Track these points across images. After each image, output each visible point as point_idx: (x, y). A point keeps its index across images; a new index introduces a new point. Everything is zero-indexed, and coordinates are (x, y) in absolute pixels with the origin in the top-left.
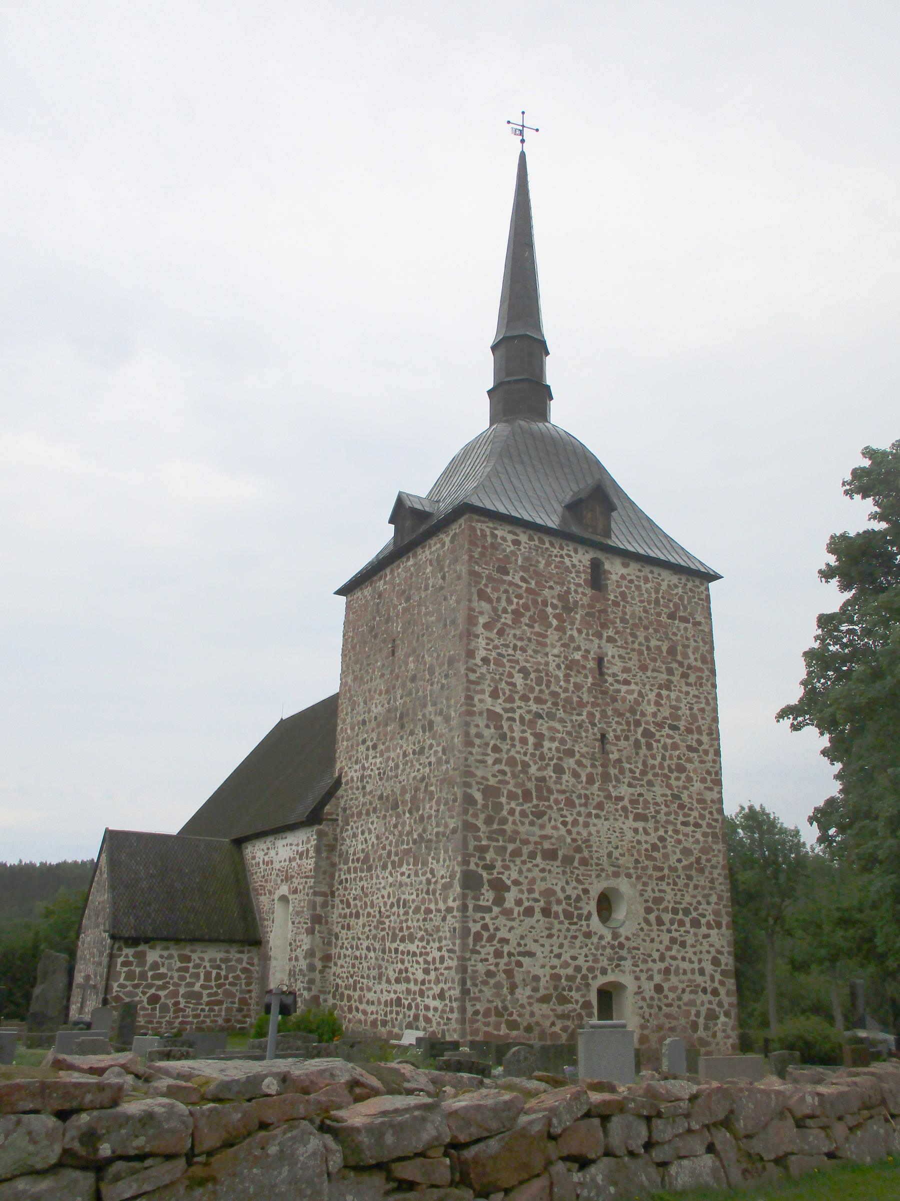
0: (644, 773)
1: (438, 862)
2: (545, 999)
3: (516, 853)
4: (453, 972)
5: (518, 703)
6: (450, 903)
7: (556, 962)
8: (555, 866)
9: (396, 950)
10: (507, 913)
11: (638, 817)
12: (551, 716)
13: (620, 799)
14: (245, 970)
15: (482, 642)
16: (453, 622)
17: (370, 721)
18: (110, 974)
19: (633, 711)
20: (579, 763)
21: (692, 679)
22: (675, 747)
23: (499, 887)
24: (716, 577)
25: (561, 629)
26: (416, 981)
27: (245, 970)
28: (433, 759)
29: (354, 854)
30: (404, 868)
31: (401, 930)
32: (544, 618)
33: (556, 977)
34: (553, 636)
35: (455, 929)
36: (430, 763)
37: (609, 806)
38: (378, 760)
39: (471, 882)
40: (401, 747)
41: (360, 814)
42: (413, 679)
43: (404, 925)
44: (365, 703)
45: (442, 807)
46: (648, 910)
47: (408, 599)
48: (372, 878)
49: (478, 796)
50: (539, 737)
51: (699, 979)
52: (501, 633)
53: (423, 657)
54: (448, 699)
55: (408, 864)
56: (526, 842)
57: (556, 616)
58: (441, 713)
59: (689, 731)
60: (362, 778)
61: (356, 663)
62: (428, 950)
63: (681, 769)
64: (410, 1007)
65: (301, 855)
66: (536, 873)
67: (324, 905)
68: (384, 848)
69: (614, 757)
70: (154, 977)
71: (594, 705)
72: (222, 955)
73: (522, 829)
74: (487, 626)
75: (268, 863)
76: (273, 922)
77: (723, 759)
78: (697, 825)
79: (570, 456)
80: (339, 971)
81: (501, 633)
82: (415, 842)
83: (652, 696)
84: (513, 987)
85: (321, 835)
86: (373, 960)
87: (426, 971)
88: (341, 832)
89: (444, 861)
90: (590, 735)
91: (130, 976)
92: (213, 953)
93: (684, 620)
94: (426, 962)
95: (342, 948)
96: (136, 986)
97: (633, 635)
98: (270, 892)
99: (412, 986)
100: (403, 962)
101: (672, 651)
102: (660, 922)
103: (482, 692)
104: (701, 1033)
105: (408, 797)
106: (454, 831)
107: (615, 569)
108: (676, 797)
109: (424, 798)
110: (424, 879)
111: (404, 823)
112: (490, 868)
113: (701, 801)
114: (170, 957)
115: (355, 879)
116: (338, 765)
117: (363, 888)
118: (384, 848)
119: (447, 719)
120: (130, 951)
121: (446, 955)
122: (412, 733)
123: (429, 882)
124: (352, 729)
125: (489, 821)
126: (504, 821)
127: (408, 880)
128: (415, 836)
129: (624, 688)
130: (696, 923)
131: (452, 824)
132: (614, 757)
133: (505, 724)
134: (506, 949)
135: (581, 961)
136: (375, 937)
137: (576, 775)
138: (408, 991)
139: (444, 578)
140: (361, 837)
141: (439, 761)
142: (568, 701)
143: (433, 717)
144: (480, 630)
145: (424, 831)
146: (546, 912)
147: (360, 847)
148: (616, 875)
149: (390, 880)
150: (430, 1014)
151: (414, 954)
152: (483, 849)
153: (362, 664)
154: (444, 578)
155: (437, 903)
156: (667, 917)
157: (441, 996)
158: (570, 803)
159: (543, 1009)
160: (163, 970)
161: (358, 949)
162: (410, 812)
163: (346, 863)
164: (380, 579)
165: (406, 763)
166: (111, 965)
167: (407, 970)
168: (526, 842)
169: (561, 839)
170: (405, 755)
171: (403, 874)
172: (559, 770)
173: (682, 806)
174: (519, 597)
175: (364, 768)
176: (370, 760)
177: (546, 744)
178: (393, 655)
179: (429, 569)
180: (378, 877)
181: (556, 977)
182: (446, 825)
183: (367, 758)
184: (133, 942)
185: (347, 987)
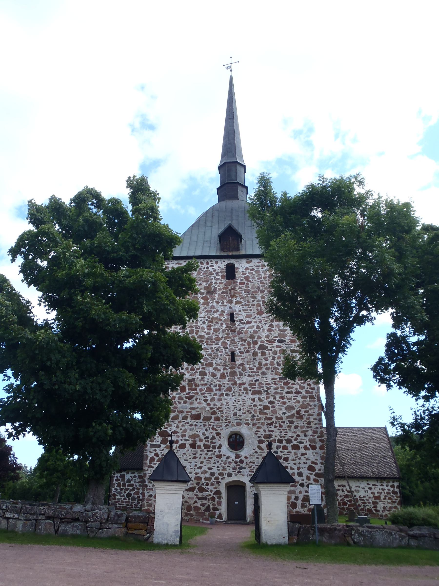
70: (128, 486)
91: (119, 485)
96: (121, 490)
114: (135, 477)
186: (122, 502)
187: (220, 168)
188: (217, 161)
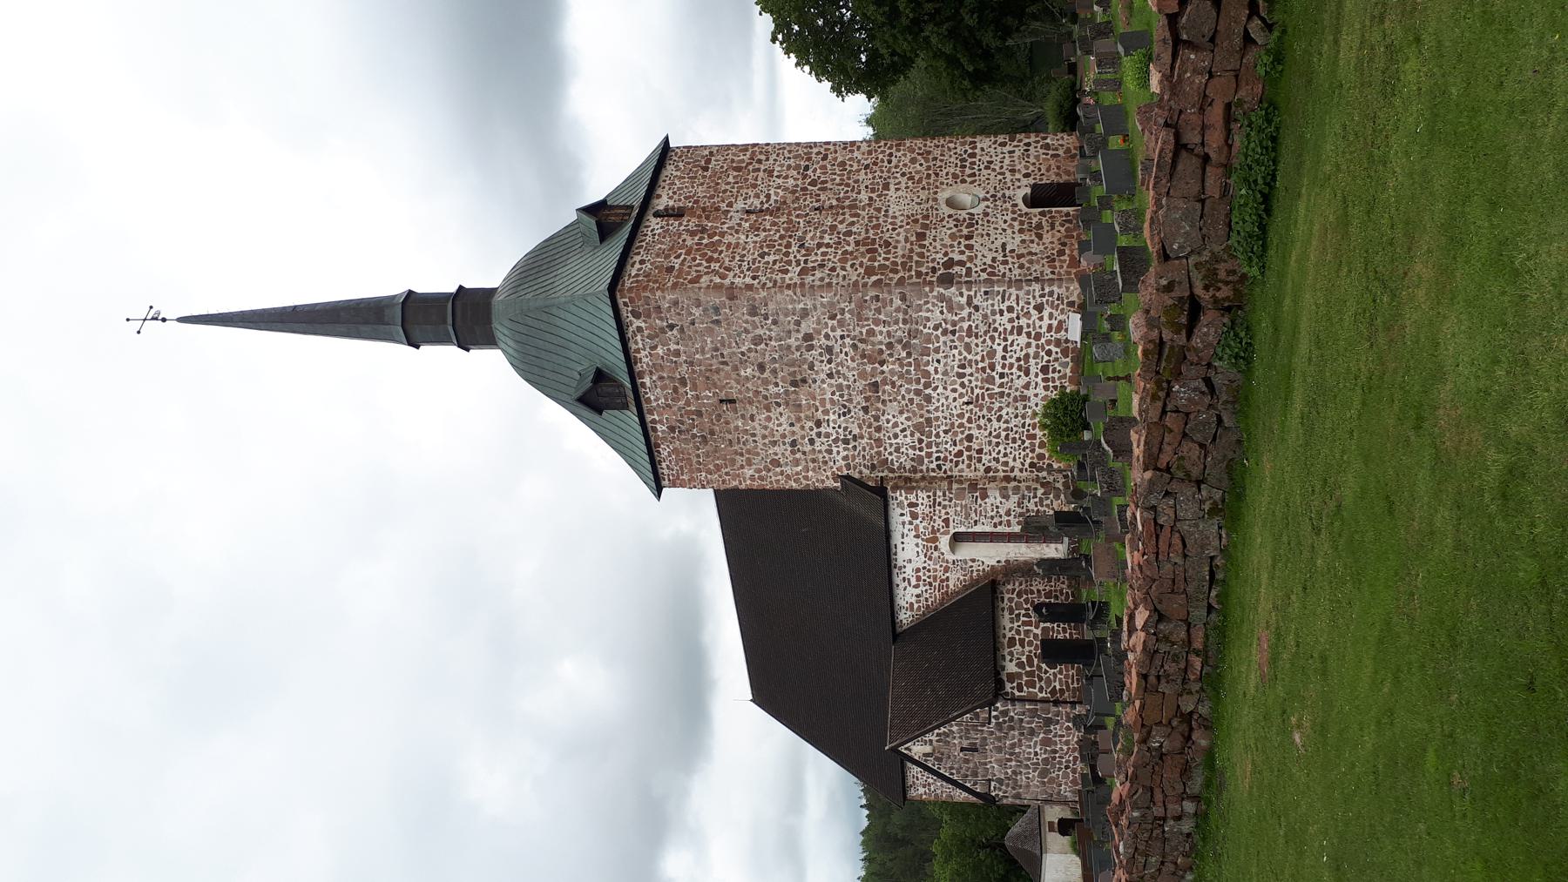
0: (848, 185)
1: (928, 319)
2: (1040, 237)
3: (921, 255)
4: (1021, 293)
5: (791, 257)
6: (964, 300)
7: (1009, 231)
8: (930, 234)
9: (1002, 376)
10: (971, 259)
11: (886, 187)
12: (801, 239)
13: (871, 199)
14: (1019, 595)
15: (737, 280)
16: (717, 310)
17: (793, 433)
18: (1033, 701)
19: (794, 192)
20: (841, 222)
21: (763, 157)
22: (824, 167)
23: (950, 263)
24: (667, 138)
25: (722, 234)
26: (1028, 345)
27: (1019, 595)
28: (839, 333)
29: (914, 448)
30: (931, 369)
31: (983, 369)
32: (713, 246)
33: (1021, 231)
34: (728, 239)
35: (986, 293)
36: (842, 337)
37: (878, 204)
38: (832, 417)
39: (947, 280)
40: (823, 381)
41: (879, 442)
42: (762, 367)
43: (981, 365)
44: (774, 443)
45: (882, 317)
46: (964, 181)
47: (683, 382)
48: (937, 419)
49: (874, 278)
50: (819, 246)
51: (1017, 153)
52: (728, 269)
53: (743, 354)
54: (786, 315)
55: (928, 363)
56: (911, 251)
57: (710, 237)
58: (798, 323)
59: (809, 159)
60: (846, 442)
61: (733, 461)
62: (1001, 329)
63: (843, 164)
64: (1049, 353)
65: (914, 516)
66: (938, 244)
67: (960, 482)
68: (911, 401)
69: (835, 203)
70: (1031, 665)
71: (790, 214)
72: (1006, 613)
73: (900, 253)
74: (723, 277)
75: (918, 579)
76: (973, 561)
77: (832, 140)
78: (891, 155)
79: (538, 266)
80: (1018, 464)
81: (728, 269)
82: (909, 355)
83: (780, 181)
84: (1030, 253)
85: (895, 488)
86: (1011, 410)
87: (1020, 330)
88: (892, 471)
89: (928, 310)
90: (816, 217)
91: (1031, 684)
92: (1005, 620)
93: (708, 161)
94: (1011, 333)
95: (997, 460)
96: (1041, 679)
97: (725, 191)
98: (946, 570)
99: (1031, 351)
100: (1011, 366)
101: (738, 169)
102: (973, 175)
103: (783, 279)
104: (1061, 152)
105: (869, 368)
106: (903, 299)
107: (663, 201)
108: (867, 167)
109: (873, 344)
110: (942, 339)
111: (892, 372)
112: (934, 270)
113: (870, 153)
114: (1011, 654)
115: (937, 445)
116: (831, 483)
117: (946, 432)
118: (911, 401)
119: (805, 313)
120: (1008, 686)
121: (1007, 303)
122: (811, 367)
123: (945, 332)
124: (797, 463)
125: (897, 272)
126: (895, 263)
127: (943, 361)
128: (904, 354)
129: (773, 197)
130: (973, 155)
131: (897, 302)
132: (835, 203)
133: (810, 265)
134: (1000, 258)
135: (1008, 218)
136: (990, 409)
137: (853, 224)
138: (1036, 356)
139: (671, 327)
140: (902, 449)
141: (841, 323)
142: (787, 230)
143: (800, 336)
144: (727, 282)
145: (899, 341)
146: (969, 237)
147: (908, 440)
148: (935, 200)
149: (940, 390)
150: (1055, 323)
151: (1005, 349)
152: (919, 274)
153: (736, 453)
154: (671, 327)
155: (963, 320)
156: (968, 171)
157: (1039, 308)
158: (877, 227)
159: (1047, 238)
160: (1024, 659)
161: (998, 436)
162: (882, 363)
163: (920, 460)
164: (655, 430)
165: (838, 372)
166: (1022, 700)
167: (1019, 359)
168: (911, 251)
169: (907, 231)
170: (830, 376)
171: (936, 371)
172: (849, 233)
173: (875, 164)
174: (694, 259)
175: (836, 441)
176: (830, 430)
177: (826, 241)
178: (733, 401)
179: (660, 351)
180: (937, 409)
181: (1021, 231)
182: (898, 310)
183: (828, 435)
184: (1000, 684)
185: (1033, 451)
186: (1067, 676)
187: (417, 347)
188: (399, 352)
